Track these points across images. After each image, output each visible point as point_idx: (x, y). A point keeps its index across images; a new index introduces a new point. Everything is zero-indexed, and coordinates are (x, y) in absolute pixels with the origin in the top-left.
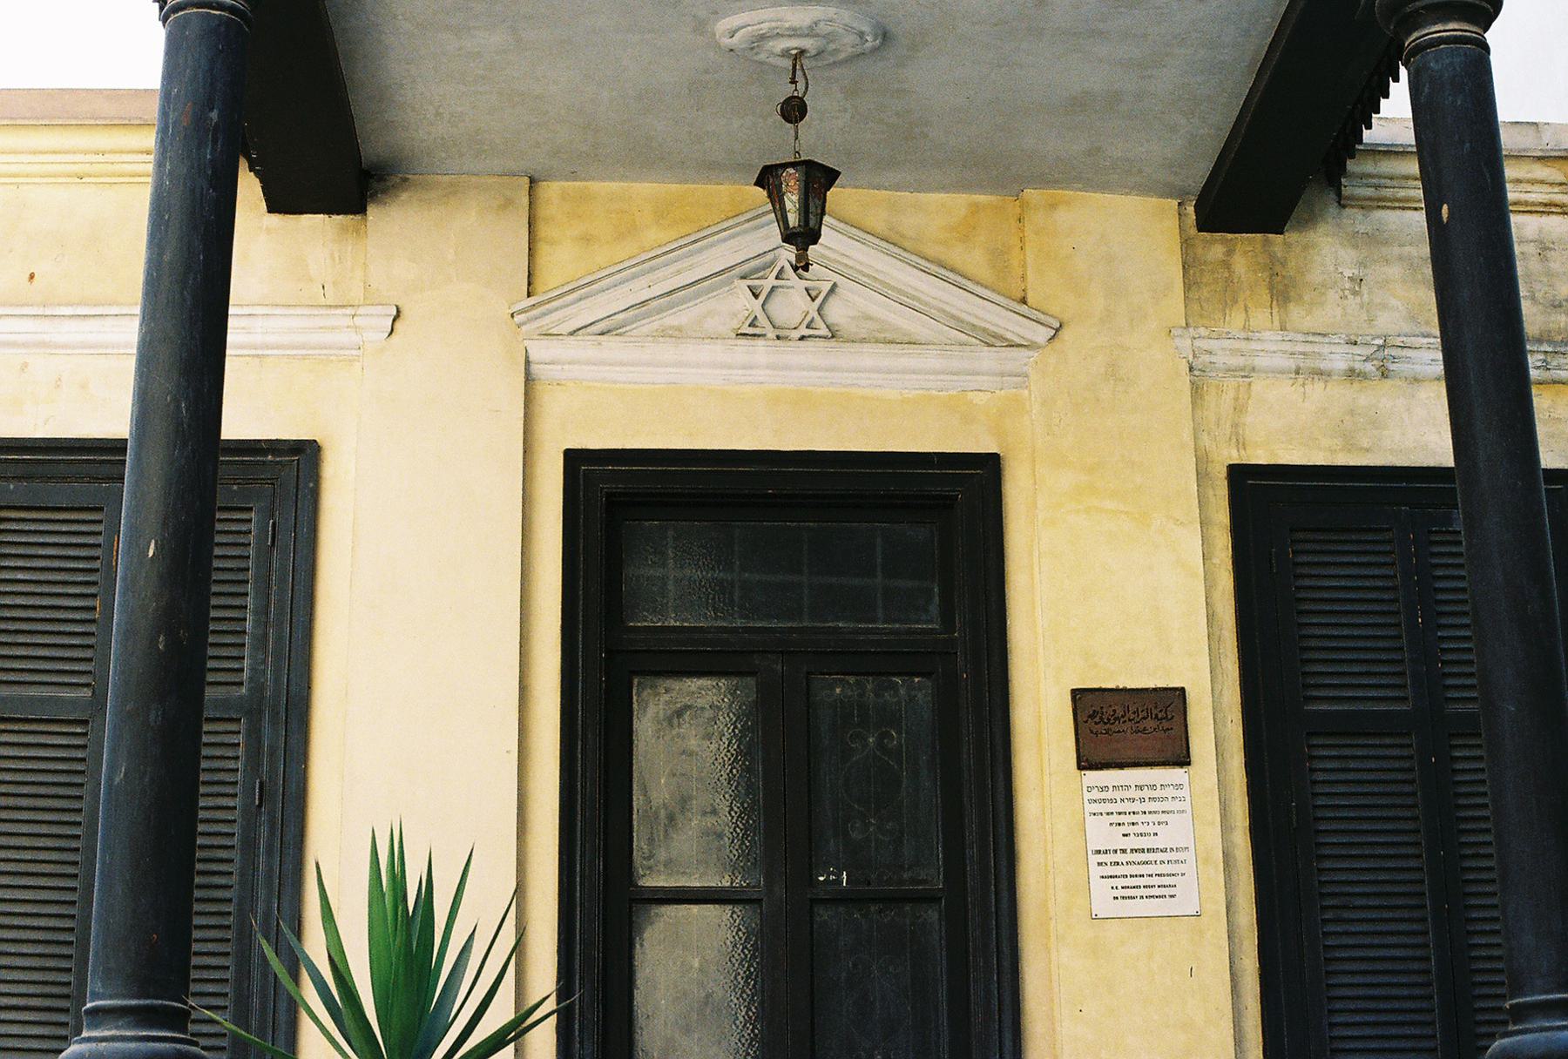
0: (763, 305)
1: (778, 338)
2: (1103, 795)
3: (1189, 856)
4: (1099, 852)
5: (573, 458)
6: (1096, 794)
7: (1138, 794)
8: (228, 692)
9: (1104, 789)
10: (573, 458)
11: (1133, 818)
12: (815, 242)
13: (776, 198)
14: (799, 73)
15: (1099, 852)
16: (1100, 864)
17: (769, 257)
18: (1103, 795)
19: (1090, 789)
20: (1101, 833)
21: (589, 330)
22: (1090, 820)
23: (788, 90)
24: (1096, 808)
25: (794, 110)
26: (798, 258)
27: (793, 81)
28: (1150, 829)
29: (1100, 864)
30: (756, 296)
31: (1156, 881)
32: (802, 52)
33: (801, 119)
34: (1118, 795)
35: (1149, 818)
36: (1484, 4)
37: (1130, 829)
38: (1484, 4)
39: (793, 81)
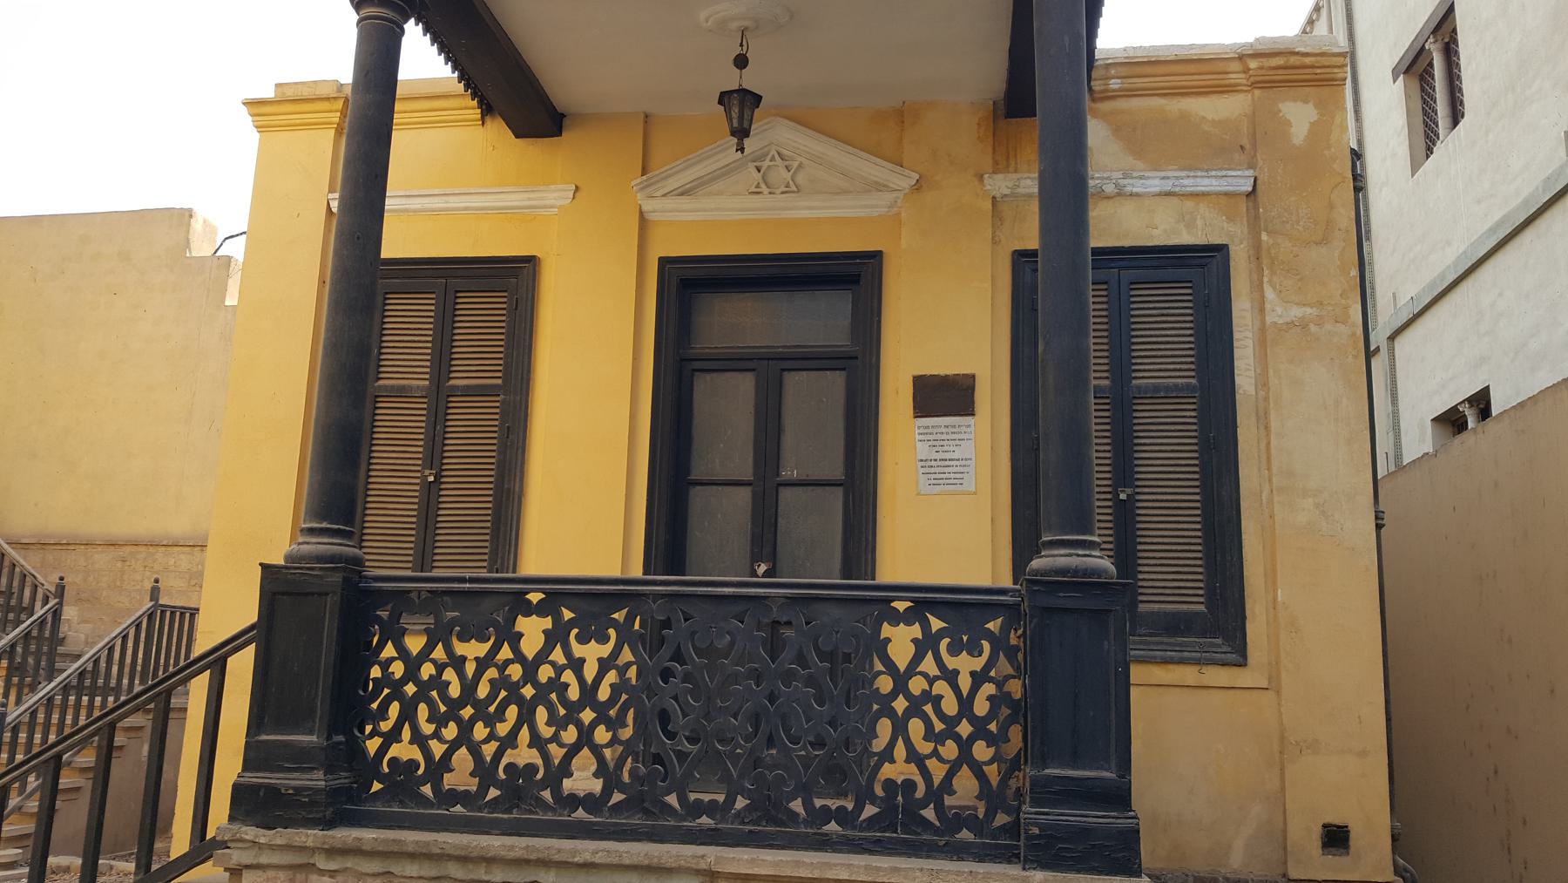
0: (792, 176)
1: (770, 193)
2: (926, 431)
3: (972, 463)
4: (922, 460)
5: (664, 262)
6: (922, 431)
7: (944, 430)
8: (1055, 561)
9: (927, 427)
10: (664, 262)
11: (942, 443)
12: (748, 136)
13: (728, 112)
14: (744, 40)
15: (922, 460)
16: (922, 467)
17: (766, 149)
18: (926, 431)
19: (919, 428)
20: (923, 450)
21: (674, 193)
22: (919, 445)
23: (738, 51)
24: (921, 437)
25: (741, 62)
26: (738, 144)
27: (741, 45)
28: (951, 448)
29: (922, 467)
30: (759, 171)
31: (952, 476)
32: (746, 28)
33: (745, 68)
34: (935, 431)
35: (950, 442)
36: (399, 2)
37: (940, 449)
38: (399, 2)
39: (741, 45)
